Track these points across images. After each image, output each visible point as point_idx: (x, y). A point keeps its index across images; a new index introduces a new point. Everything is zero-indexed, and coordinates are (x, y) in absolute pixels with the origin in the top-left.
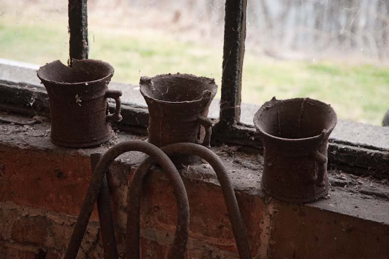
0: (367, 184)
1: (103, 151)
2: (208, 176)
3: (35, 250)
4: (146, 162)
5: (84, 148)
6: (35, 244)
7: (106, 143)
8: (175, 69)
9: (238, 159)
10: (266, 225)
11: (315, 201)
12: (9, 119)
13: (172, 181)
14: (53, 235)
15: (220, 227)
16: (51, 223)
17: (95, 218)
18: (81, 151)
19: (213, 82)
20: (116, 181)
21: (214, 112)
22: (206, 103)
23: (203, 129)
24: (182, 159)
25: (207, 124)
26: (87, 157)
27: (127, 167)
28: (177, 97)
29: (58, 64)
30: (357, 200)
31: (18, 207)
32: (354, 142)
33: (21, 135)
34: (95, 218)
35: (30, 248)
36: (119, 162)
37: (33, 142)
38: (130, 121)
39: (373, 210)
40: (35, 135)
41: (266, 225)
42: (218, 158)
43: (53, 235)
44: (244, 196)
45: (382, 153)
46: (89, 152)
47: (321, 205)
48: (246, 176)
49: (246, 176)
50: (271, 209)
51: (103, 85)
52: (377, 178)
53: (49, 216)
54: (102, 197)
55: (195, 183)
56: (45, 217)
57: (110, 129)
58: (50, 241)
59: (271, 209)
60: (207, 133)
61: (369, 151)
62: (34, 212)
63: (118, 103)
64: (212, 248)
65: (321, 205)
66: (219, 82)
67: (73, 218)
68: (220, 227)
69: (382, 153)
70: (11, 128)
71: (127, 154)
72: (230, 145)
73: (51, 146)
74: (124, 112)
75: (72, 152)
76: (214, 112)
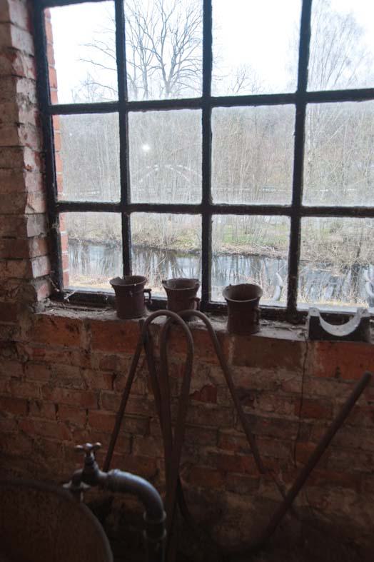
0: (277, 324)
1: (145, 319)
2: (200, 326)
3: (112, 373)
4: (167, 323)
5: (135, 318)
6: (112, 370)
7: (145, 316)
8: (348, 323)
9: (213, 318)
10: (231, 347)
11: (254, 333)
12: (95, 309)
13: (183, 328)
14: (120, 364)
15: (208, 352)
16: (119, 359)
17: (143, 354)
18: (134, 320)
19: (198, 280)
20: (152, 333)
21: (199, 295)
22: (196, 289)
23: (196, 303)
24: (187, 318)
25: (198, 300)
26: (136, 323)
27: (157, 326)
28: (180, 292)
29: (119, 278)
30: (275, 331)
31: (102, 352)
32: (268, 305)
33: (102, 315)
34: (143, 354)
35: (109, 373)
36: (153, 324)
37: (109, 318)
38: (156, 305)
39: (333, 150)
40: (107, 315)
41: (231, 347)
42: (206, 316)
43: (120, 364)
44: (220, 333)
45: (37, 248)
46: (138, 320)
47: (258, 334)
48: (220, 325)
49: (220, 325)
50: (233, 339)
51: (143, 286)
52: (281, 321)
53: (118, 355)
54: (146, 343)
55: (195, 329)
56: (115, 356)
57: (146, 308)
58: (119, 368)
59: (233, 339)
60: (198, 304)
61: (276, 308)
62: (110, 354)
63: (150, 294)
64: (203, 363)
65: (258, 334)
66: (200, 280)
67: (132, 354)
68: (208, 352)
69: (37, 248)
70: (96, 313)
71: (158, 317)
72: (208, 312)
73: (118, 319)
74: (153, 300)
75: (128, 321)
76: (199, 295)
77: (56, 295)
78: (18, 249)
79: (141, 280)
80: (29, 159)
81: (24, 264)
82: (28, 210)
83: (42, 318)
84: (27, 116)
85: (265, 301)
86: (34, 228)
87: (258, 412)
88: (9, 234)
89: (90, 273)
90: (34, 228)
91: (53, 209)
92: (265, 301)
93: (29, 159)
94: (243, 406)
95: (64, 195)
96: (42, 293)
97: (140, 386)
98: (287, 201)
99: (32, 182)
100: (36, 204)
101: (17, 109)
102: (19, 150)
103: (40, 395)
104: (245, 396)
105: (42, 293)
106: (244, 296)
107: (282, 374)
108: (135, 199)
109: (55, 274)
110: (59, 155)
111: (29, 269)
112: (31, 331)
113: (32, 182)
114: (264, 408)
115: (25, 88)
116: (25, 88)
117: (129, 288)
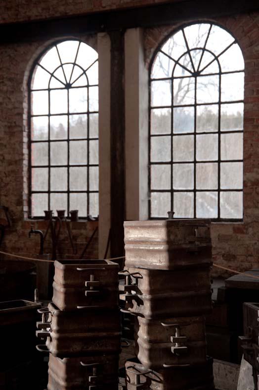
44: (68, 222)
45: (25, 203)
69: (25, 203)
77: (29, 217)
78: (20, 203)
79: (52, 211)
80: (25, 179)
81: (21, 207)
82: (24, 193)
83: (25, 222)
84: (25, 169)
85: (80, 215)
86: (25, 197)
87: (78, 243)
88: (147, 64)
89: (38, 210)
90: (25, 197)
91: (31, 193)
92: (80, 215)
93: (25, 179)
94: (218, 366)
95: (33, 189)
96: (26, 216)
97: (48, 238)
98: (47, 194)
99: (25, 186)
100: (26, 191)
101: (22, 167)
102: (22, 178)
103: (22, 245)
104: (75, 238)
105: (26, 216)
106: (75, 213)
107: (83, 231)
108: (221, 164)
109: (30, 212)
110: (84, 97)
111: (23, 208)
112: (22, 226)
113: (25, 186)
114: (79, 241)
115: (25, 162)
116: (25, 162)
117: (48, 213)
